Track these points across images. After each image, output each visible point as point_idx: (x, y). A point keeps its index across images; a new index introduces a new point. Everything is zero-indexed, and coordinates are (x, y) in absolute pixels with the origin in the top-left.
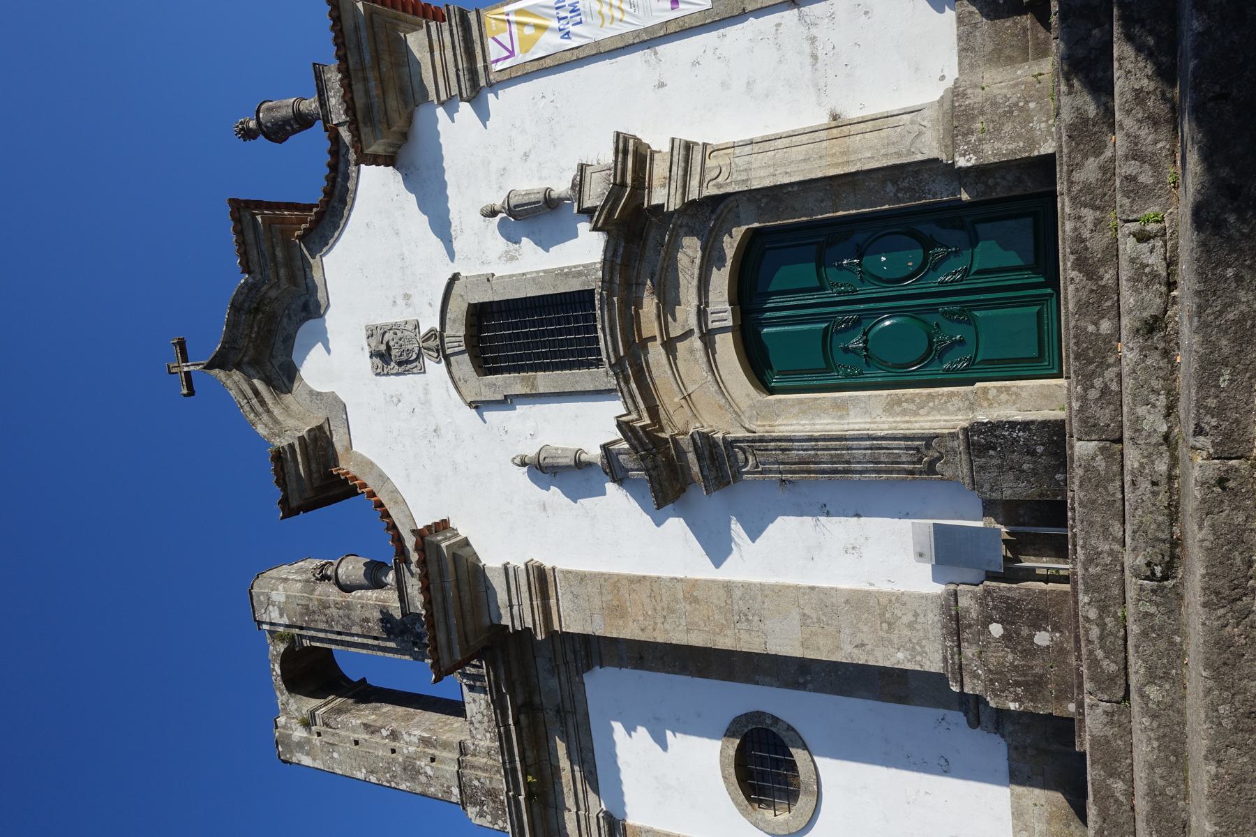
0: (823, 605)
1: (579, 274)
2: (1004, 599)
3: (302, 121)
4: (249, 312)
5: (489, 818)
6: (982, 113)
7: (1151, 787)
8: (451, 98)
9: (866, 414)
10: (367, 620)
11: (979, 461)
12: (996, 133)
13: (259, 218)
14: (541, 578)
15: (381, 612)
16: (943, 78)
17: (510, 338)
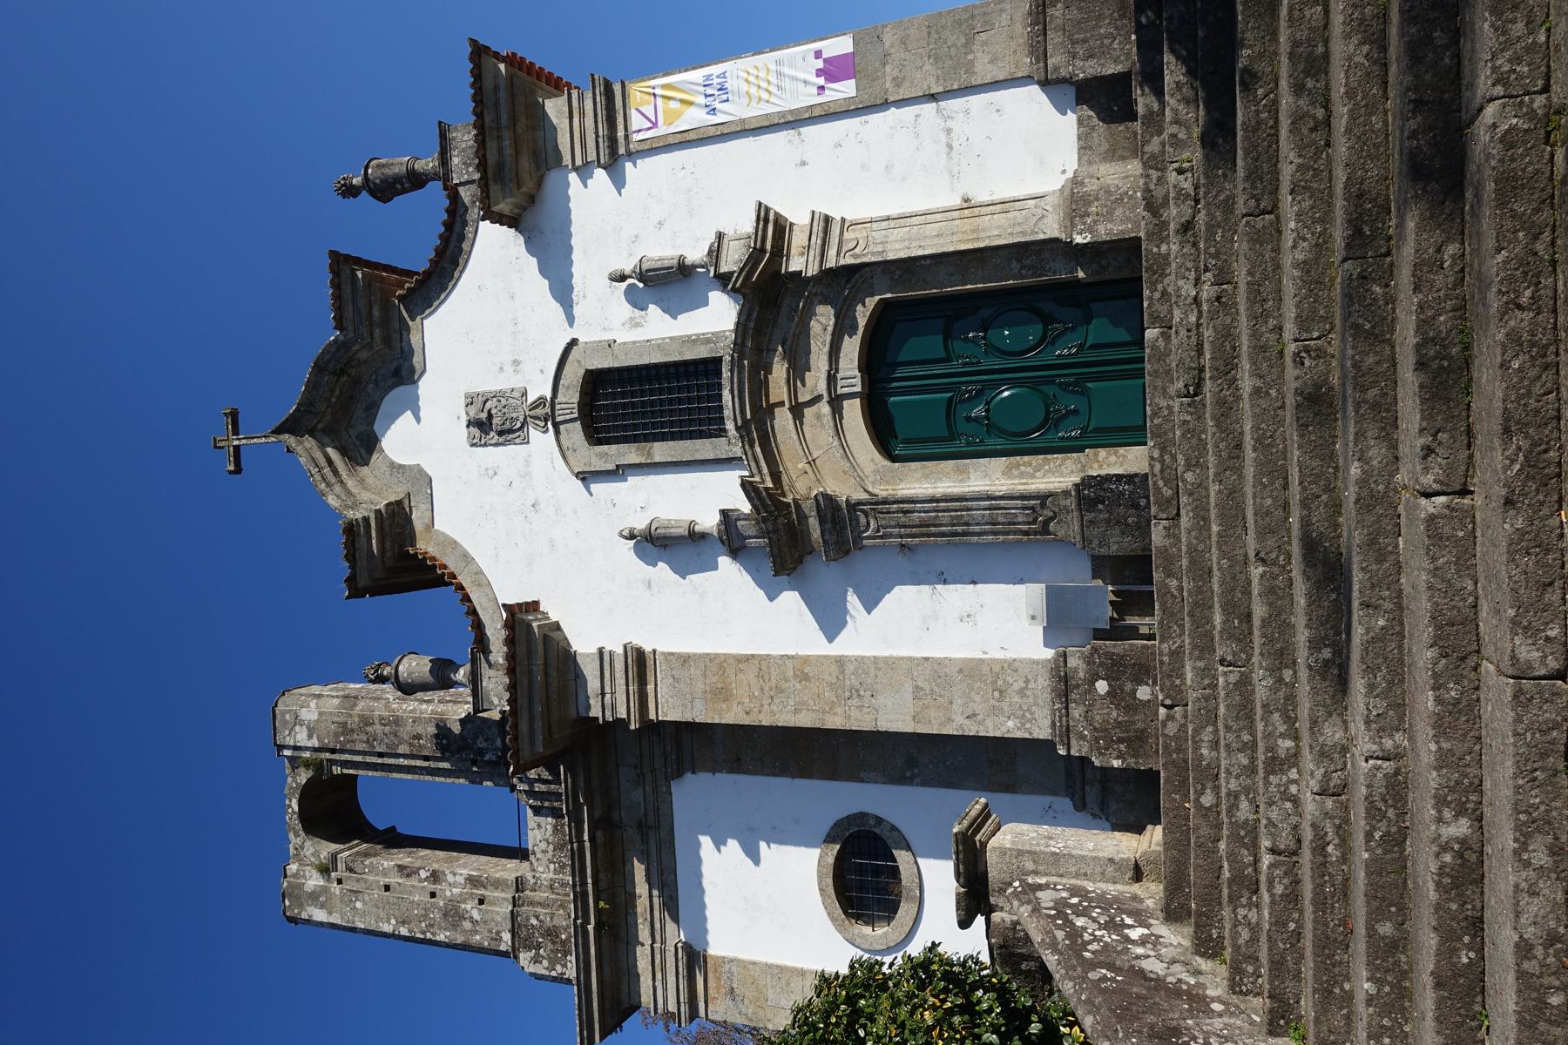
0: (936, 676)
1: (708, 341)
2: (1110, 655)
3: (415, 180)
4: (335, 373)
5: (545, 963)
6: (1097, 199)
7: (1189, 545)
8: (586, 164)
9: (989, 477)
10: (418, 737)
11: (1089, 516)
12: (1109, 216)
13: (359, 274)
14: (640, 662)
15: (437, 726)
16: (1064, 172)
17: (627, 408)
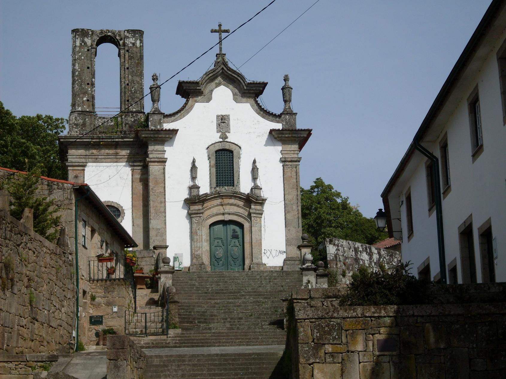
14: (163, 161)
17: (224, 160)
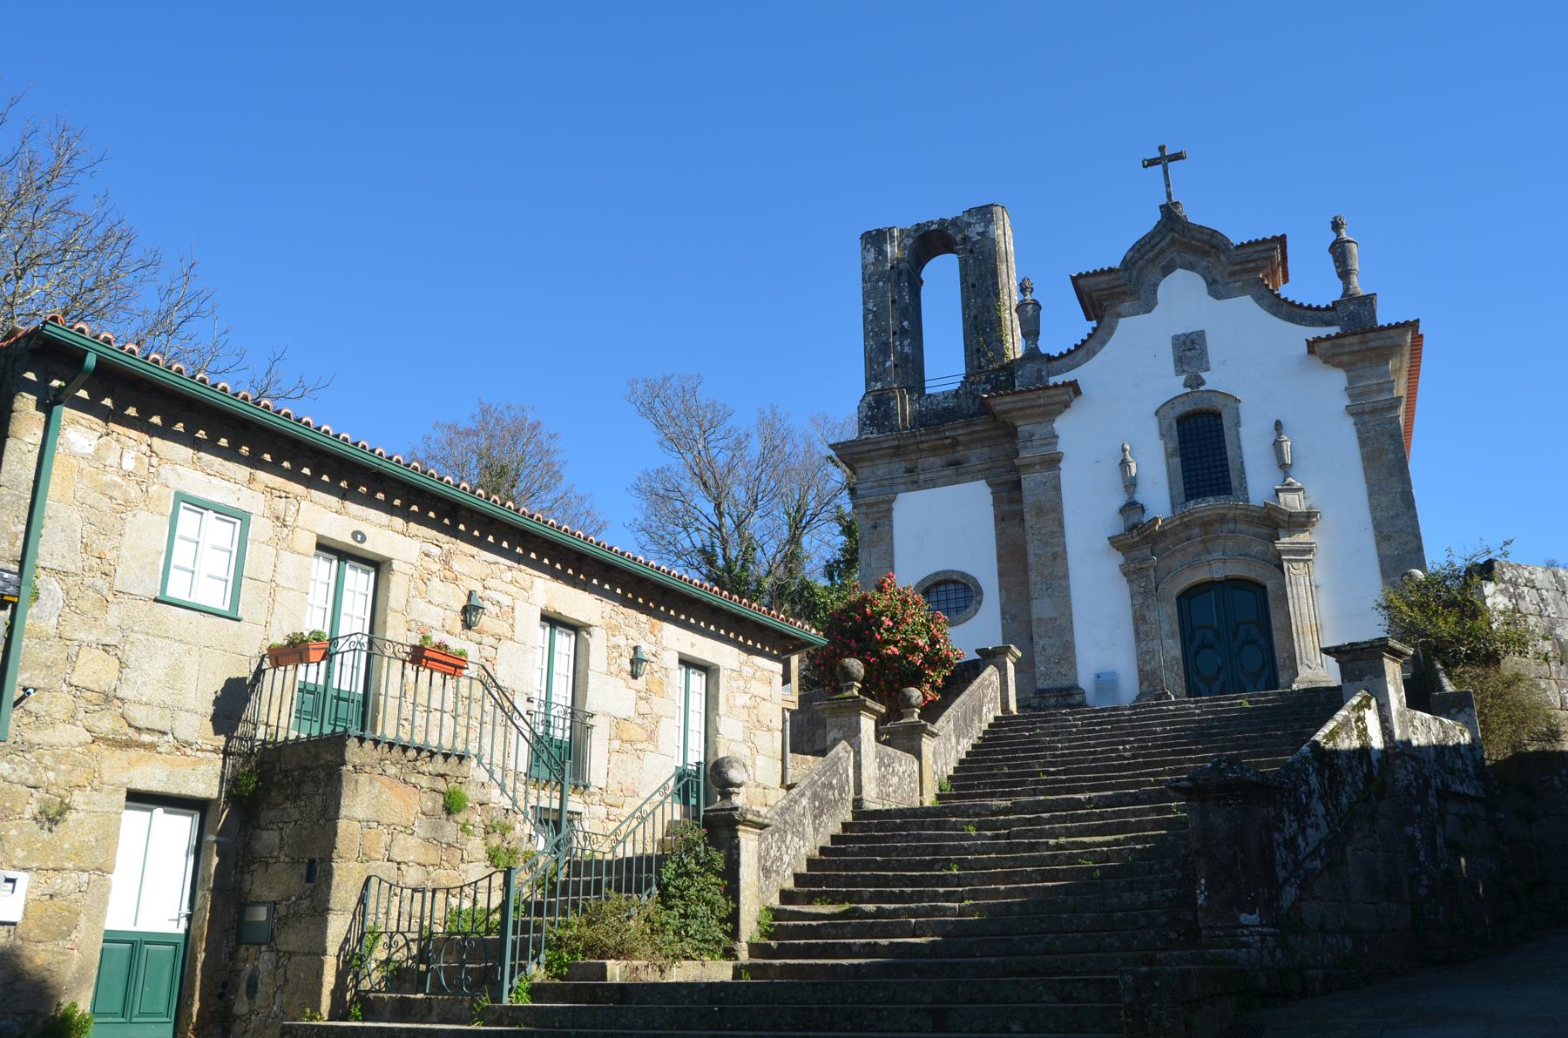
17: (1201, 441)
